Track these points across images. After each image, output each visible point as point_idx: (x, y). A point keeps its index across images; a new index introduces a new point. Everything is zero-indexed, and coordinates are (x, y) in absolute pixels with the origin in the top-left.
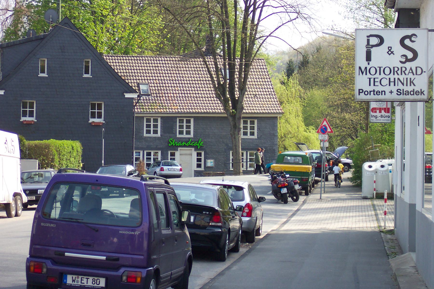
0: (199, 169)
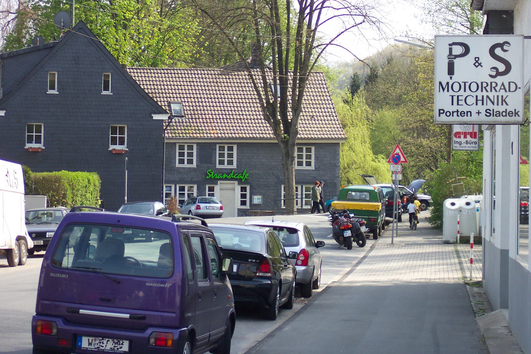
0: (243, 207)
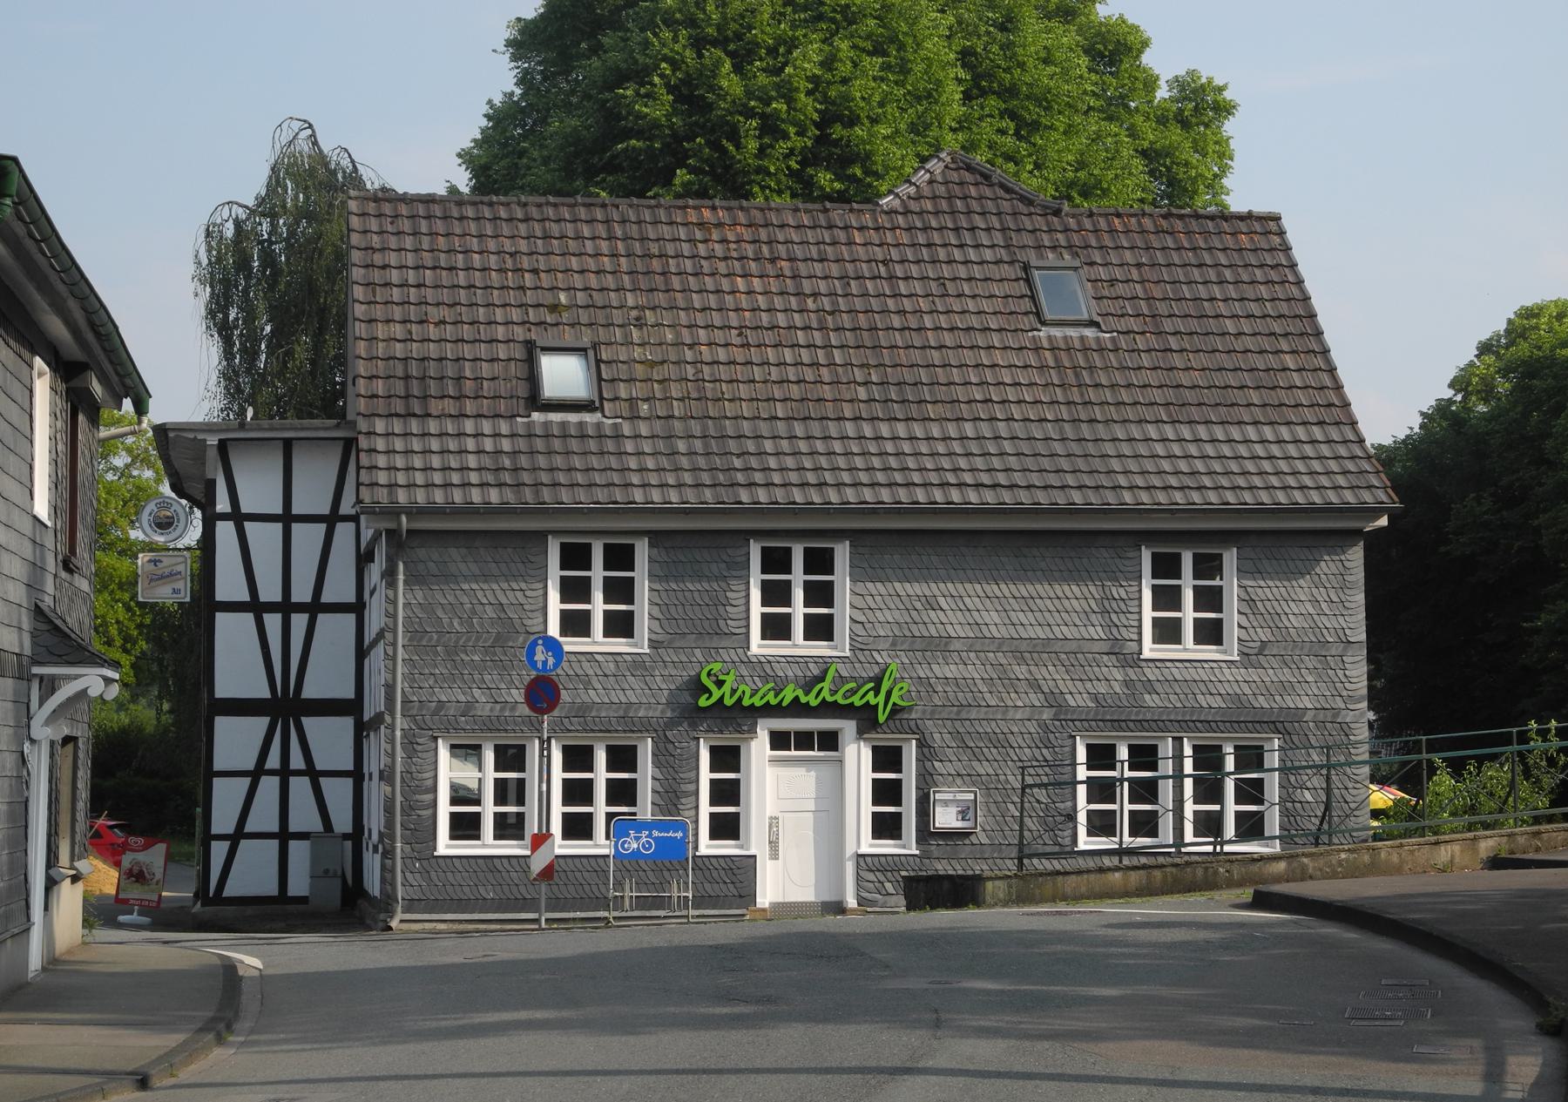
0: (887, 847)
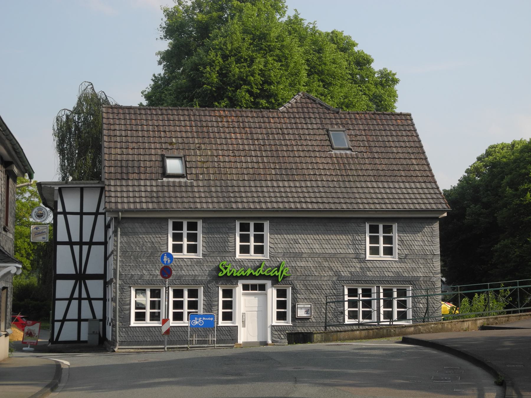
0: (282, 323)
